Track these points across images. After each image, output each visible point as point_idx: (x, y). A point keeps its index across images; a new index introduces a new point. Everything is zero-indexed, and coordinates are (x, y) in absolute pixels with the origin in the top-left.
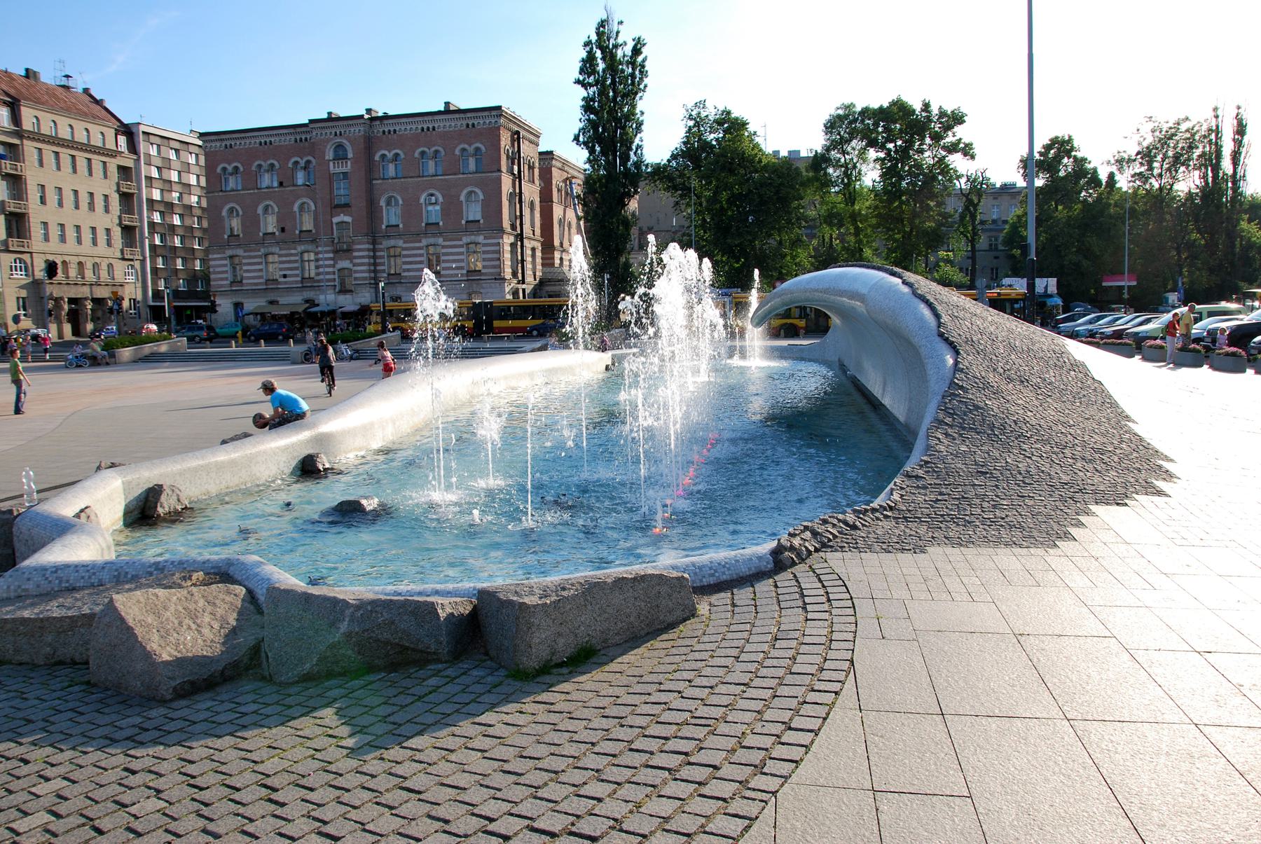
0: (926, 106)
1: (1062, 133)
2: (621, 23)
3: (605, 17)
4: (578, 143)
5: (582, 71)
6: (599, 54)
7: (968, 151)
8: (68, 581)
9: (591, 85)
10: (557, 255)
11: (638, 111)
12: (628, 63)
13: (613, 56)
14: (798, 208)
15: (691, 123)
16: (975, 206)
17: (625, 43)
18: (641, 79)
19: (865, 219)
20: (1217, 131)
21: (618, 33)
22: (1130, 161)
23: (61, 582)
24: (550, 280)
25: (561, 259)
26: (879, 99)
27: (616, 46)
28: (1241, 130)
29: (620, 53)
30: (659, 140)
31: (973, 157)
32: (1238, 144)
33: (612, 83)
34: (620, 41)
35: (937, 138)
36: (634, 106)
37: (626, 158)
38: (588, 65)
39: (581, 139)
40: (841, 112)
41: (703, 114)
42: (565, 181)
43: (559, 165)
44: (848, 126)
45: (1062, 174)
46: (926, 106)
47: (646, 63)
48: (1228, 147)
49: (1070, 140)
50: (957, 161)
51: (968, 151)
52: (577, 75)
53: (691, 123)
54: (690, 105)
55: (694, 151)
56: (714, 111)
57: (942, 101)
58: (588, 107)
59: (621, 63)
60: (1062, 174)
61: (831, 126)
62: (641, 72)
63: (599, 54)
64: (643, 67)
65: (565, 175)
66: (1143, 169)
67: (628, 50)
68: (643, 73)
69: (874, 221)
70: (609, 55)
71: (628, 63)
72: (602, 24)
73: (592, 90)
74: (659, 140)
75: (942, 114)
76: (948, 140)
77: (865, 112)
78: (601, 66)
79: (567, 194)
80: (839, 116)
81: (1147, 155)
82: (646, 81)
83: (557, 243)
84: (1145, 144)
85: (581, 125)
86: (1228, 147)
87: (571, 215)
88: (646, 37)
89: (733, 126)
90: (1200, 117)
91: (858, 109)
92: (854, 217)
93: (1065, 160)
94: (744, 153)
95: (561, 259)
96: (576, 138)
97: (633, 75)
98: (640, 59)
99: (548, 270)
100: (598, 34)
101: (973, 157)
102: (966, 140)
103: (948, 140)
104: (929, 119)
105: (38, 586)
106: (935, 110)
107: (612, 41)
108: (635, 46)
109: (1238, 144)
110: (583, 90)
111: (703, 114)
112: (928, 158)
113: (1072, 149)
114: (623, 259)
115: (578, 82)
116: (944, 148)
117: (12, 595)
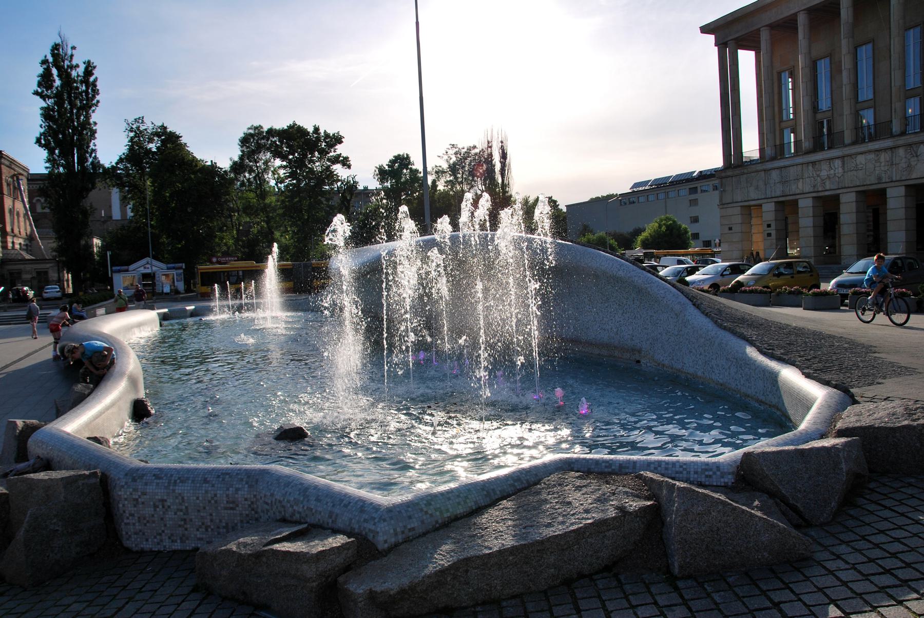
0: (316, 130)
1: (401, 152)
2: (74, 48)
3: (58, 41)
4: (41, 145)
5: (40, 84)
6: (55, 71)
7: (345, 163)
8: (448, 511)
9: (49, 97)
10: (9, 239)
11: (91, 121)
12: (82, 82)
13: (69, 75)
14: (227, 201)
15: (132, 134)
16: (349, 201)
17: (77, 66)
18: (94, 97)
19: (274, 210)
20: (491, 155)
21: (72, 56)
22: (443, 172)
23: (441, 512)
24: (11, 260)
25: (13, 243)
26: (281, 124)
27: (71, 67)
28: (504, 156)
29: (74, 74)
30: (109, 148)
31: (349, 167)
32: (503, 165)
33: (68, 98)
34: (74, 63)
35: (323, 153)
36: (88, 117)
37: (82, 160)
38: (45, 80)
39: (43, 142)
40: (252, 131)
41: (142, 128)
42: (12, 177)
43: (7, 163)
44: (255, 142)
45: (403, 180)
46: (316, 130)
47: (98, 83)
48: (498, 167)
49: (408, 157)
50: (338, 169)
51: (345, 163)
52: (35, 87)
53: (132, 134)
54: (131, 120)
55: (135, 154)
56: (151, 126)
57: (329, 127)
58: (47, 114)
59: (75, 81)
60: (403, 180)
61: (245, 141)
62: (93, 91)
63: (55, 71)
64: (95, 86)
65: (13, 172)
66: (451, 178)
67: (81, 70)
68: (96, 92)
69: (281, 211)
70: (65, 74)
71: (82, 82)
72: (56, 47)
73: (50, 102)
74: (109, 148)
75: (327, 135)
76: (331, 154)
77: (271, 132)
78: (58, 83)
79: (15, 188)
80: (251, 135)
81: (453, 169)
82: (98, 98)
83: (8, 229)
84: (451, 162)
85: (42, 130)
86: (498, 167)
87: (19, 206)
88: (95, 61)
89: (170, 140)
90: (481, 145)
91: (265, 129)
92: (265, 209)
93: (405, 171)
94: (183, 159)
95: (13, 243)
96: (38, 141)
97: (87, 92)
98: (92, 79)
99: (5, 251)
100: (53, 55)
101: (349, 167)
102: (344, 155)
103: (331, 154)
104: (318, 139)
105: (423, 522)
106: (322, 131)
107: (67, 63)
108: (86, 69)
109: (503, 165)
110: (41, 100)
111: (142, 128)
112: (317, 167)
113: (409, 163)
114: (83, 242)
115: (36, 93)
116: (329, 160)
117: (400, 538)
